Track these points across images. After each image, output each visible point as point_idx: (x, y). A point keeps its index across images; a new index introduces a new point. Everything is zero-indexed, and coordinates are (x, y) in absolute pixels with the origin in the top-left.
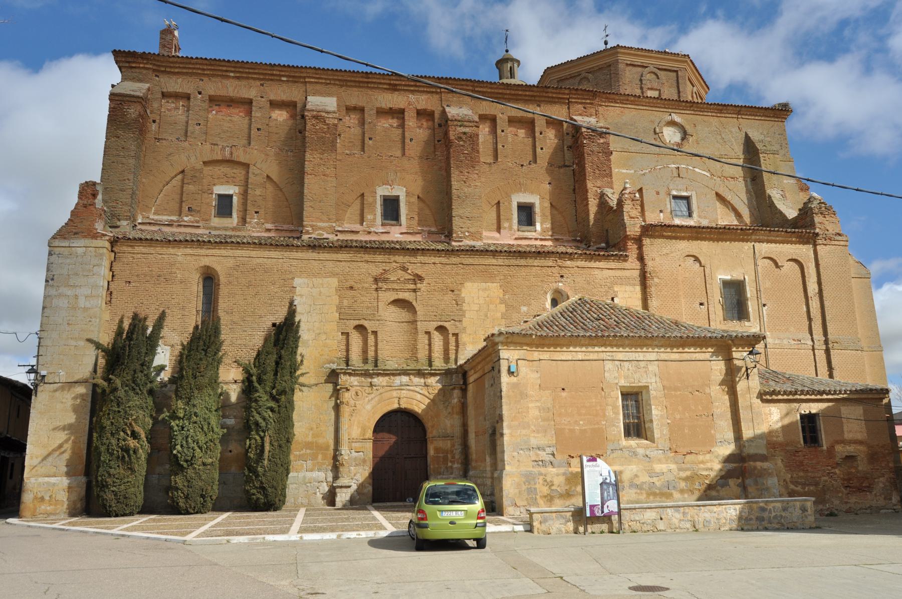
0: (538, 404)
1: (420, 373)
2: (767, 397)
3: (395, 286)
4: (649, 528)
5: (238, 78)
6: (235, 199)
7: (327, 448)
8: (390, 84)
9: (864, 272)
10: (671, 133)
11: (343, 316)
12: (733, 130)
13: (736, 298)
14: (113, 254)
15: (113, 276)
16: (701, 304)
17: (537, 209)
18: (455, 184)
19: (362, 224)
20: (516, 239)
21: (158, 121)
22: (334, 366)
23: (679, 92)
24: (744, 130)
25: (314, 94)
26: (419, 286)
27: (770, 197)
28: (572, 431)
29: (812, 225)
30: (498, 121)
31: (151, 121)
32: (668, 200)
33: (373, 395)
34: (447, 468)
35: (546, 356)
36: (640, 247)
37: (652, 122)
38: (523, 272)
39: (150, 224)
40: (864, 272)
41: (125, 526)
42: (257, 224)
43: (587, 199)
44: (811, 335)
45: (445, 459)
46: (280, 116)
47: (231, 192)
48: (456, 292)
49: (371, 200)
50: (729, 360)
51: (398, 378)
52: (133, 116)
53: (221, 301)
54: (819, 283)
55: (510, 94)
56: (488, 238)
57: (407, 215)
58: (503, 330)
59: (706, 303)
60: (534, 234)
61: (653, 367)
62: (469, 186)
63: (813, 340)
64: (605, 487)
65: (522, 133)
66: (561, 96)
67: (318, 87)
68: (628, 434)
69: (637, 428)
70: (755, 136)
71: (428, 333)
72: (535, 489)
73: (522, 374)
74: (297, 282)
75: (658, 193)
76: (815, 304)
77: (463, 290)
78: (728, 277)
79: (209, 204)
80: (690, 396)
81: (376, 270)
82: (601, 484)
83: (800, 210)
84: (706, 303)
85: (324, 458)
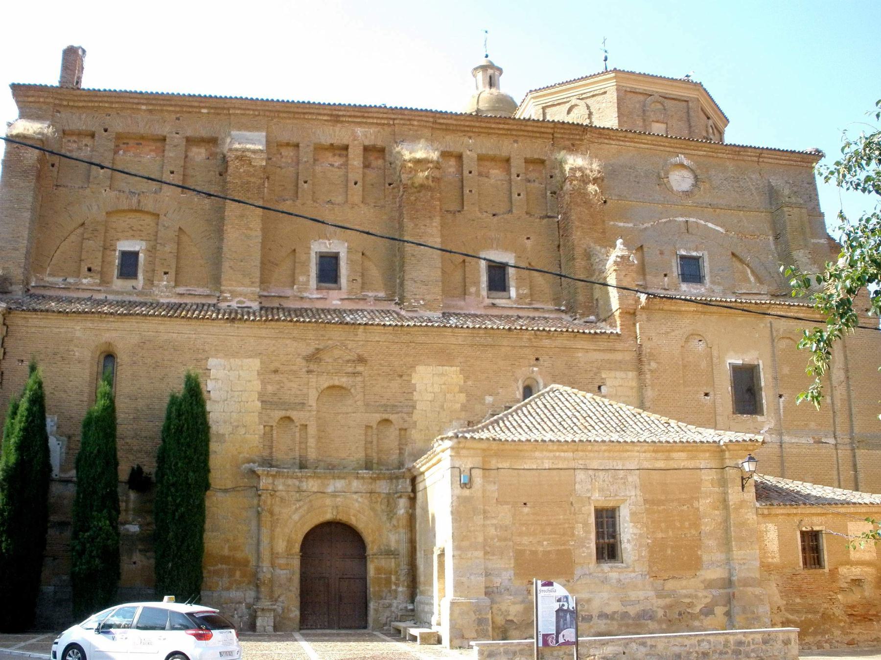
6: (141, 255)
8: (331, 115)
12: (753, 176)
15: (5, 353)
21: (57, 165)
41: (23, 644)
42: (166, 287)
45: (388, 582)
47: (137, 249)
48: (404, 378)
57: (348, 276)
64: (561, 614)
66: (543, 130)
74: (212, 362)
78: (740, 362)
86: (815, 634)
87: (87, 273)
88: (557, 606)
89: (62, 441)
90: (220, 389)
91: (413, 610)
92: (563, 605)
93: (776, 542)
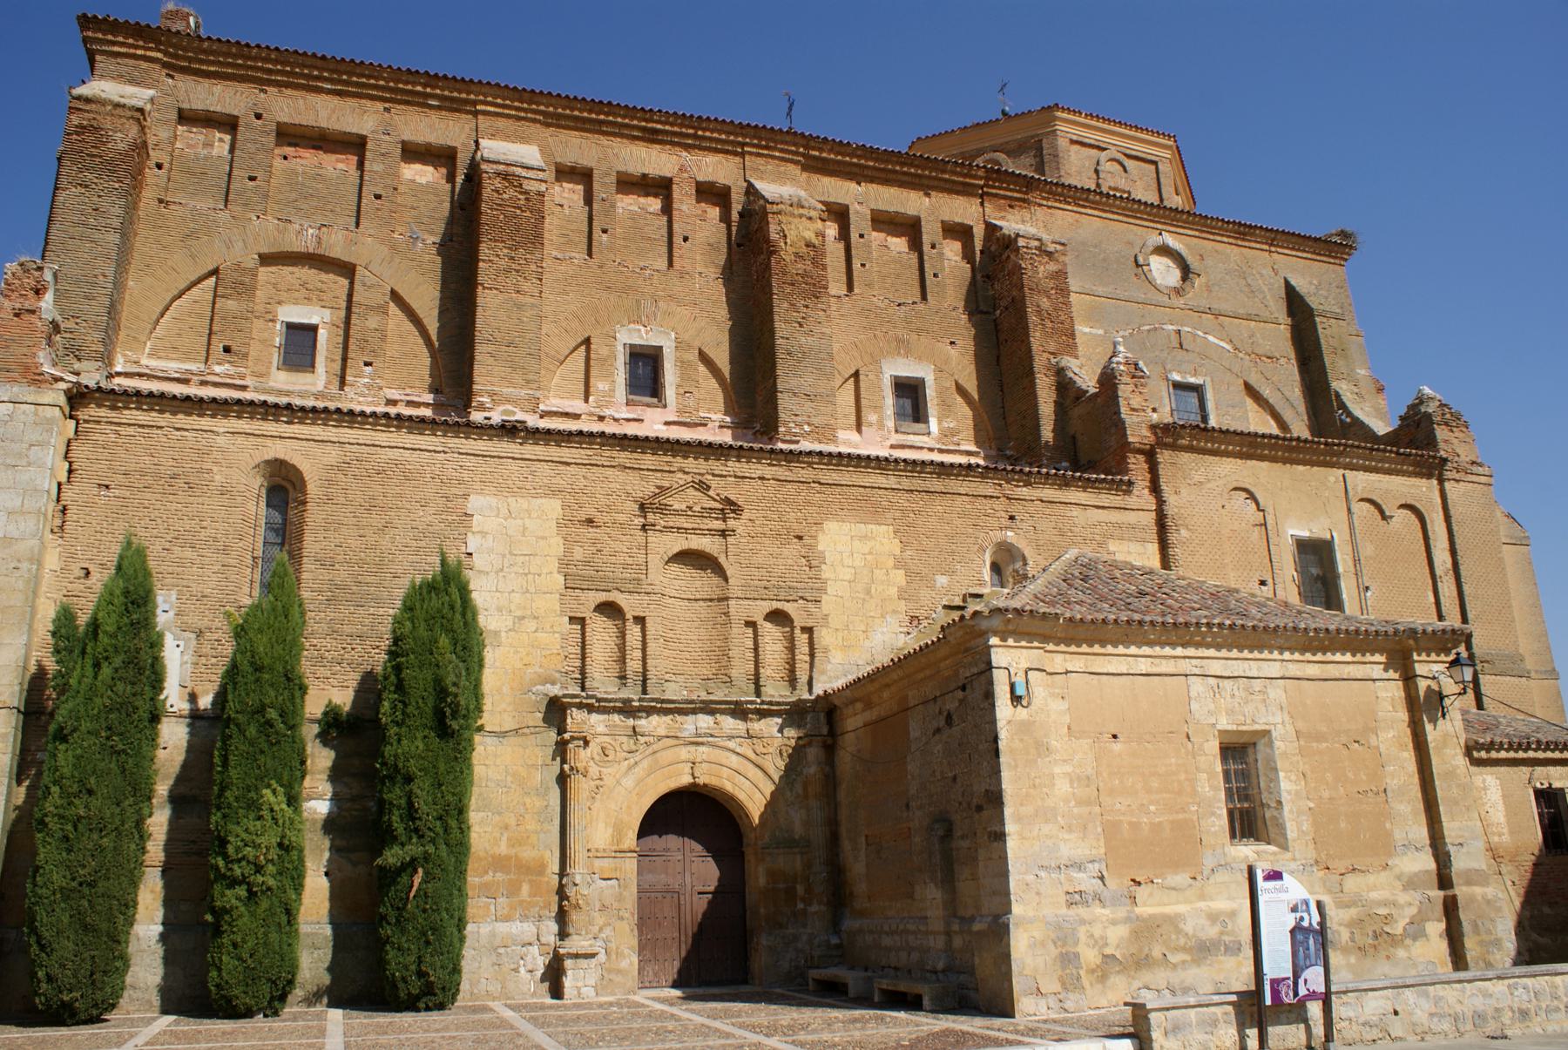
1: (739, 711)
2: (1478, 753)
3: (682, 522)
4: (1375, 1033)
5: (339, 93)
6: (322, 334)
7: (541, 868)
8: (644, 129)
9: (1518, 533)
10: (1162, 268)
11: (572, 585)
14: (73, 422)
15: (70, 471)
16: (1263, 583)
17: (930, 392)
19: (586, 401)
20: (892, 447)
22: (555, 690)
24: (1282, 274)
25: (493, 136)
26: (731, 523)
27: (1338, 395)
28: (1135, 826)
29: (1431, 442)
30: (853, 217)
31: (152, 163)
32: (1164, 388)
33: (638, 757)
35: (1077, 663)
37: (1130, 243)
38: (939, 505)
39: (140, 375)
40: (1518, 533)
42: (368, 387)
43: (1033, 373)
45: (790, 893)
46: (423, 174)
47: (314, 320)
49: (604, 351)
50: (1409, 678)
51: (691, 718)
52: (121, 146)
53: (308, 538)
54: (1453, 552)
55: (874, 168)
57: (678, 386)
59: (1270, 581)
60: (925, 438)
61: (1276, 692)
65: (899, 244)
67: (501, 123)
69: (1248, 821)
71: (751, 624)
72: (1077, 955)
74: (475, 503)
77: (820, 537)
78: (1305, 534)
80: (1345, 752)
81: (644, 487)
82: (1292, 932)
84: (1270, 581)
85: (536, 890)
87: (222, 355)
88: (1290, 921)
89: (187, 641)
91: (838, 946)
92: (1302, 919)
93: (1501, 807)
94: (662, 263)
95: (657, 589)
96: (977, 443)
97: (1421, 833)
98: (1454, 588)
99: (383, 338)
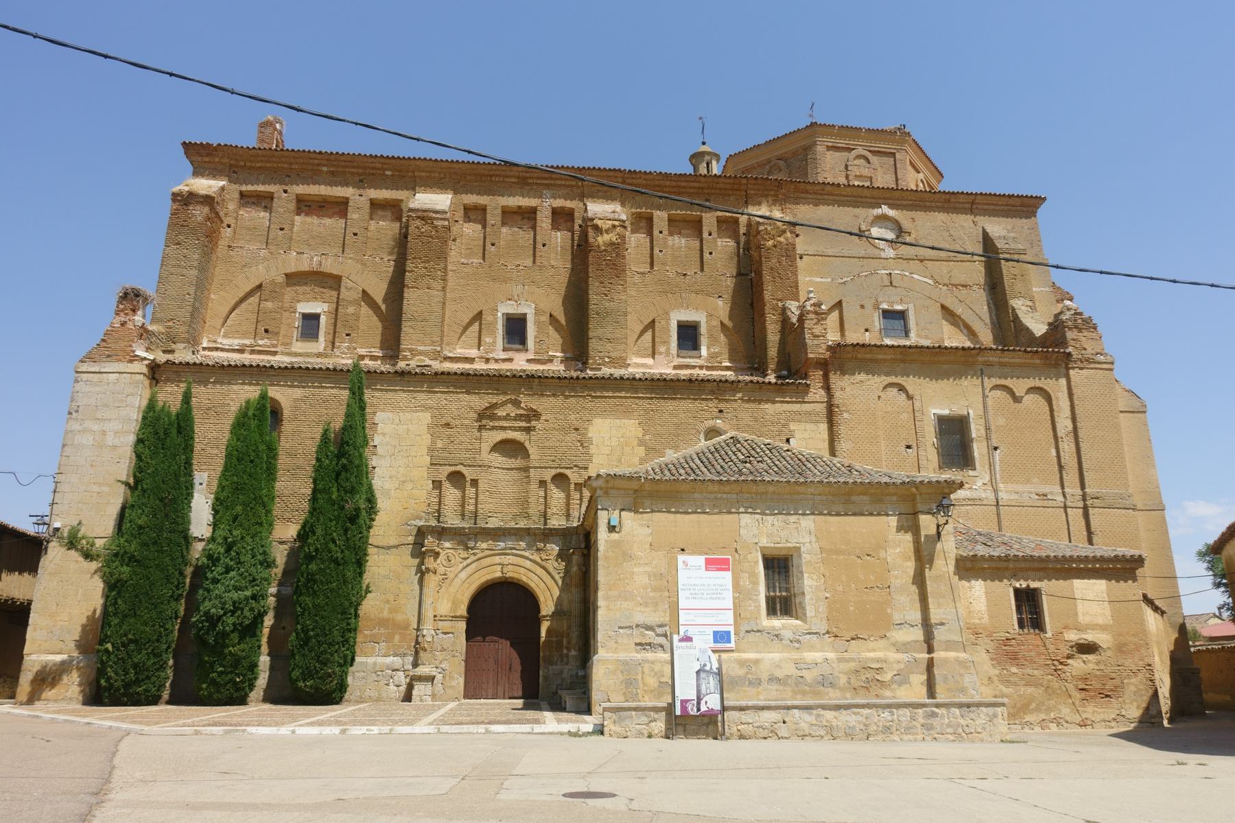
0: (648, 569)
3: (505, 424)
6: (323, 319)
8: (519, 178)
13: (955, 440)
16: (908, 447)
17: (703, 329)
18: (593, 298)
23: (897, 180)
26: (534, 423)
27: (1014, 309)
29: (1063, 342)
30: (655, 220)
32: (876, 315)
33: (468, 561)
34: (561, 656)
36: (826, 377)
40: (1136, 405)
44: (1063, 487)
45: (559, 645)
47: (318, 311)
52: (199, 218)
54: (1074, 419)
56: (638, 365)
58: (602, 472)
62: (612, 300)
63: (1064, 496)
68: (772, 610)
70: (989, 230)
71: (542, 483)
73: (625, 529)
75: (862, 307)
76: (1067, 447)
78: (946, 412)
79: (290, 326)
80: (859, 561)
83: (1050, 324)
86: (1038, 710)
90: (387, 444)
93: (983, 599)
94: (529, 262)
95: (486, 463)
96: (731, 360)
97: (916, 616)
98: (1073, 445)
99: (357, 320)
